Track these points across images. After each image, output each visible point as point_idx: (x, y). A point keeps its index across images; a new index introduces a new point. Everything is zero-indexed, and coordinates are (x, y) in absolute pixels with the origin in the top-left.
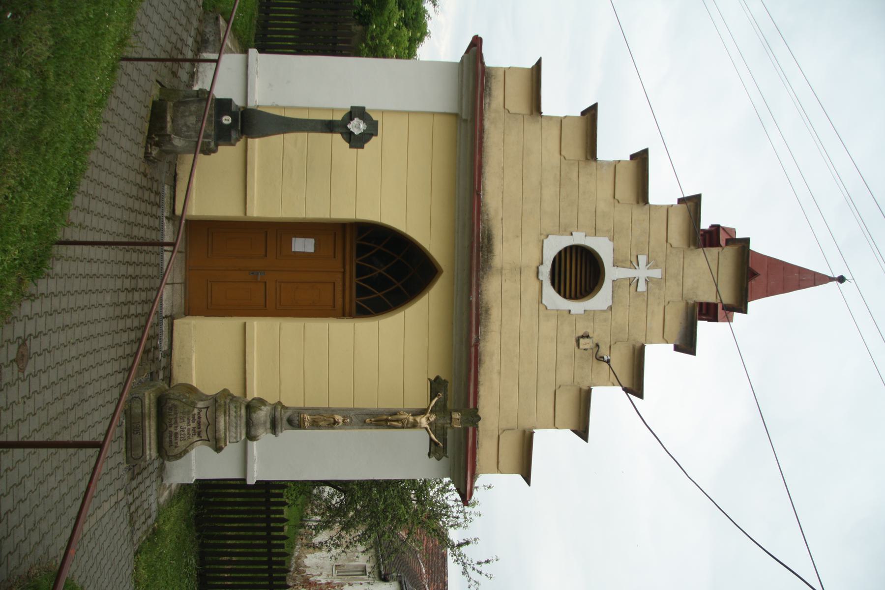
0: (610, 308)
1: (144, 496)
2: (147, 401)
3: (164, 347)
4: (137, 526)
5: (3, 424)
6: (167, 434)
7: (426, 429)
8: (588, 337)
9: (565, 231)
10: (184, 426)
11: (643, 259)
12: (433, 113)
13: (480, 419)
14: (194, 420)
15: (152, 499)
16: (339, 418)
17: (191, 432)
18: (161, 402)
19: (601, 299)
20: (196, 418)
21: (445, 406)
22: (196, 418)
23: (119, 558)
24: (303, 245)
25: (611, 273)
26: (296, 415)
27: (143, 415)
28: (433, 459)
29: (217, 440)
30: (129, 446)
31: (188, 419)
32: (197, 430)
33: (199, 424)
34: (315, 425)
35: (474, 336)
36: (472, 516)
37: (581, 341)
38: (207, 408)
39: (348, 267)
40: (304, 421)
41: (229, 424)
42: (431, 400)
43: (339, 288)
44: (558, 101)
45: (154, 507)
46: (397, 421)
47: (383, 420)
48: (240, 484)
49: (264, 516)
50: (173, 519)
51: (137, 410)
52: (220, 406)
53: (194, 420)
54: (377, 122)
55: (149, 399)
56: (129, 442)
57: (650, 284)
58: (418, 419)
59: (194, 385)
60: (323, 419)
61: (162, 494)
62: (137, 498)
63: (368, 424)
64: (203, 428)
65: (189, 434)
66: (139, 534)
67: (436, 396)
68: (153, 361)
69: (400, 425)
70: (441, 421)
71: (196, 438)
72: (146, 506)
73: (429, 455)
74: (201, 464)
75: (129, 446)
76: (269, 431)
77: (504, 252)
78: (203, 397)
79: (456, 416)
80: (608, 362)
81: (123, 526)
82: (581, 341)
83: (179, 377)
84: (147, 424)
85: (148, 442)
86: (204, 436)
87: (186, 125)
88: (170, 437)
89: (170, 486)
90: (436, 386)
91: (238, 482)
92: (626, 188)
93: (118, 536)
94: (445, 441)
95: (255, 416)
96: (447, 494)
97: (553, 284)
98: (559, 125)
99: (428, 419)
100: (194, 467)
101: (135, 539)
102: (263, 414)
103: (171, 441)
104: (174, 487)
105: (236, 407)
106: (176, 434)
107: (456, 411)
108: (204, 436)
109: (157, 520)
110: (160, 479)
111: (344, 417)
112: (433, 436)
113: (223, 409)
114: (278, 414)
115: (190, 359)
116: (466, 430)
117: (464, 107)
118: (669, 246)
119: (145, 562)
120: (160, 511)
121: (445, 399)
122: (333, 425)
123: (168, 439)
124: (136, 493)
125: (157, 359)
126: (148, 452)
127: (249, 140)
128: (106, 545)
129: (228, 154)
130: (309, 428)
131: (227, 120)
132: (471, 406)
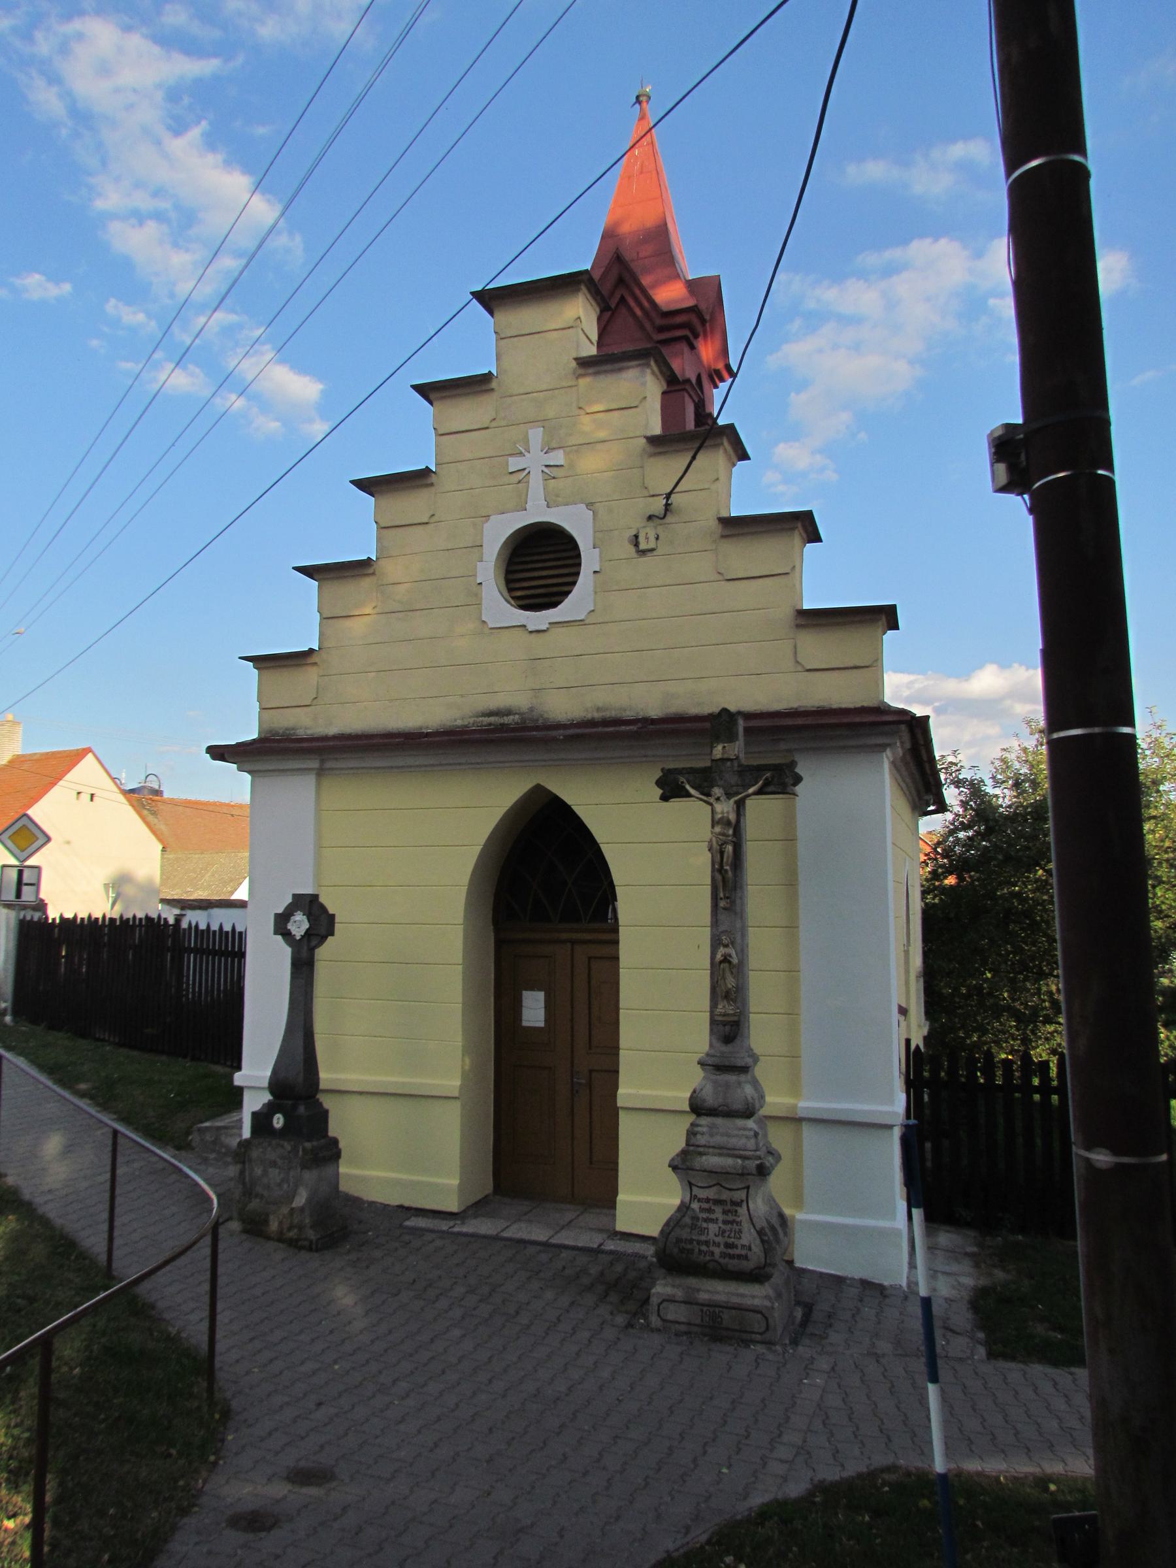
0: (590, 506)
8: (636, 537)
9: (476, 595)
11: (514, 464)
12: (318, 810)
13: (725, 710)
16: (719, 957)
17: (730, 1218)
19: (575, 522)
20: (706, 1206)
22: (706, 1206)
24: (534, 1009)
25: (537, 513)
28: (799, 789)
32: (728, 1207)
33: (718, 1202)
37: (643, 546)
38: (691, 1184)
39: (565, 936)
42: (689, 795)
44: (297, 624)
53: (709, 1211)
54: (294, 896)
57: (554, 445)
63: (733, 903)
64: (726, 1195)
69: (729, 848)
71: (742, 1211)
76: (743, 1078)
77: (509, 691)
80: (668, 496)
82: (643, 546)
86: (742, 1195)
87: (279, 1185)
88: (732, 1257)
92: (411, 505)
94: (761, 769)
97: (554, 605)
98: (330, 621)
99: (718, 799)
103: (739, 1257)
106: (727, 1245)
108: (742, 1195)
117: (389, 764)
118: (494, 424)
122: (739, 970)
126: (757, 1302)
127: (322, 1086)
129: (347, 1122)
131: (278, 1121)
132: (707, 725)
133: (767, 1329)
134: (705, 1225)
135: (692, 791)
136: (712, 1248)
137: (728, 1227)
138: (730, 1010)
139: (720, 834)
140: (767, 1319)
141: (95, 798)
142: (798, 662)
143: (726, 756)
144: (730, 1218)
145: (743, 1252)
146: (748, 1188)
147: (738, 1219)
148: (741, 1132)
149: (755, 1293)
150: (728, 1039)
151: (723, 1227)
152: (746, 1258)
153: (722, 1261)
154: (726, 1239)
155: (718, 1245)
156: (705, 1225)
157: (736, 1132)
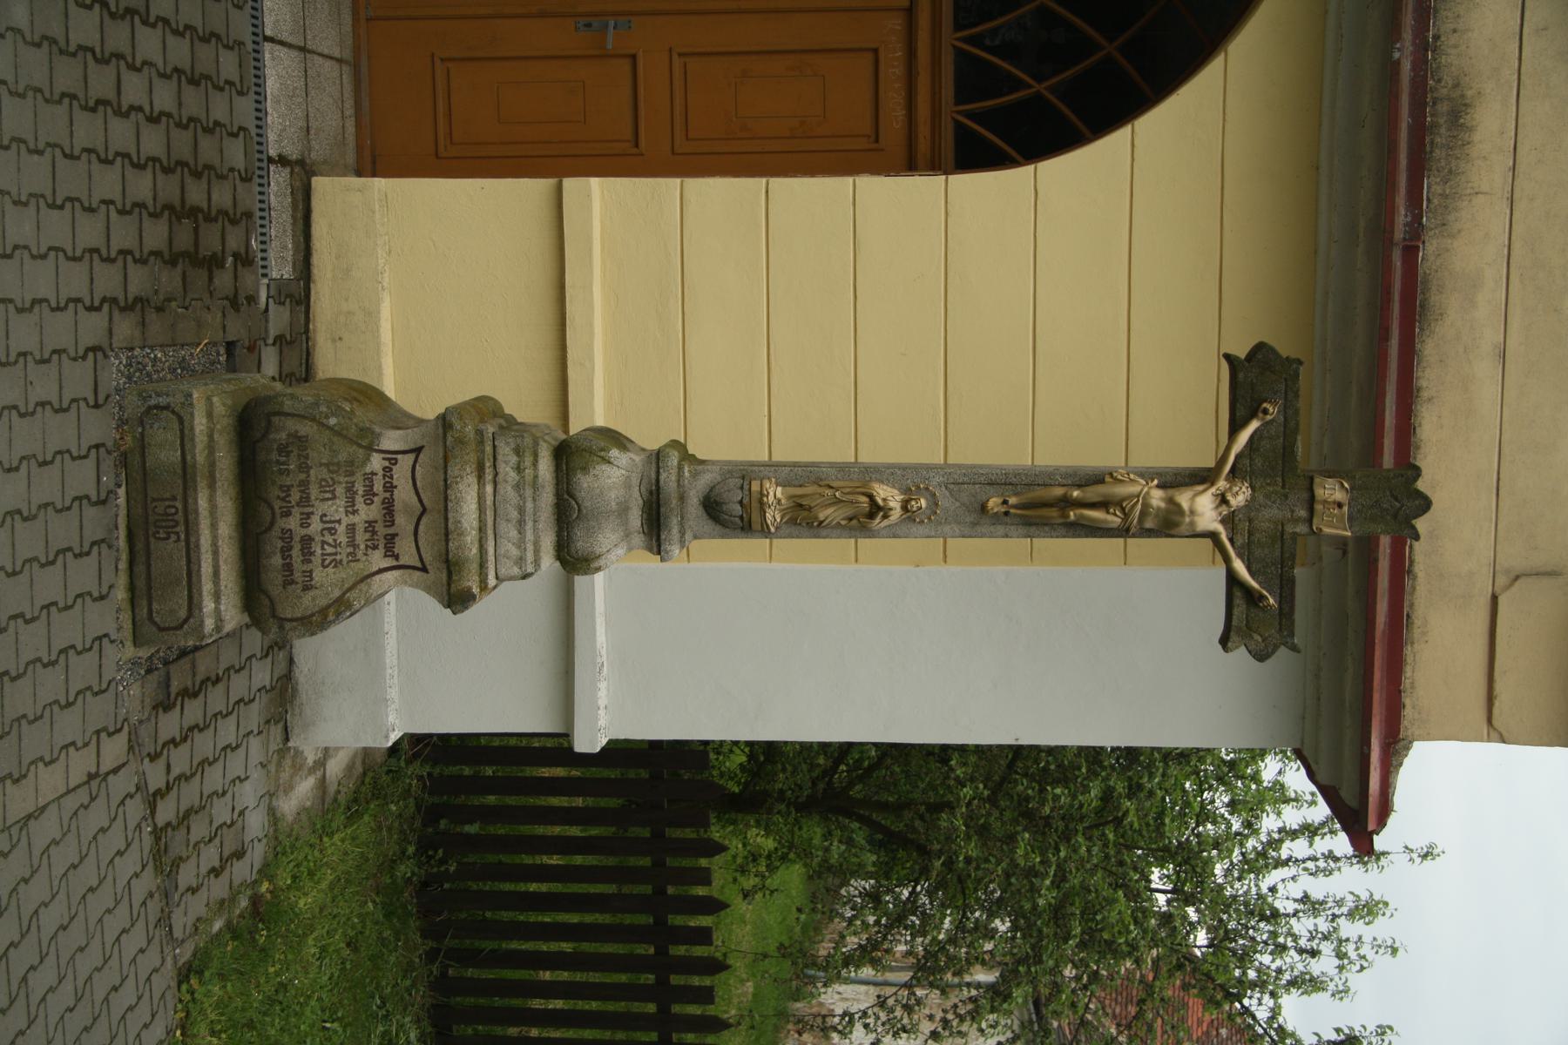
1: (214, 778)
2: (200, 423)
3: (281, 268)
4: (186, 876)
5: (10, 713)
6: (274, 542)
7: (1213, 536)
10: (335, 515)
14: (370, 494)
15: (248, 794)
16: (883, 492)
17: (361, 537)
18: (251, 426)
20: (378, 487)
21: (1288, 452)
22: (378, 487)
23: (111, 976)
26: (734, 482)
27: (186, 471)
28: (1241, 654)
29: (451, 566)
30: (141, 583)
31: (350, 490)
32: (381, 530)
33: (389, 507)
34: (802, 520)
35: (1402, 217)
36: (1366, 950)
40: (762, 506)
41: (495, 511)
42: (1235, 428)
43: (893, 69)
45: (256, 823)
46: (1104, 505)
47: (1051, 507)
48: (556, 748)
49: (647, 889)
50: (330, 876)
51: (165, 454)
52: (461, 441)
53: (370, 494)
55: (208, 411)
56: (140, 568)
58: (1184, 498)
59: (390, 390)
60: (834, 504)
61: (289, 788)
62: (184, 778)
64: (403, 523)
65: (352, 543)
66: (197, 906)
67: (1253, 415)
68: (234, 303)
69: (1114, 520)
70: (1272, 513)
71: (378, 560)
72: (221, 812)
73: (1224, 641)
74: (413, 670)
75: (141, 583)
76: (638, 539)
78: (399, 419)
79: (1331, 491)
81: (129, 864)
83: (331, 362)
84: (203, 503)
85: (206, 568)
86: (408, 556)
88: (286, 551)
89: (321, 764)
90: (1253, 379)
91: (550, 743)
93: (104, 898)
95: (589, 492)
96: (1274, 877)
99: (1223, 500)
100: (393, 693)
101: (181, 922)
102: (612, 480)
103: (288, 567)
104: (335, 767)
105: (518, 451)
106: (307, 541)
107: (1330, 474)
108: (408, 556)
109: (266, 872)
110: (276, 731)
111: (907, 491)
112: (1239, 566)
113: (473, 457)
114: (669, 480)
115: (372, 316)
116: (1366, 547)
119: (220, 1005)
120: (280, 842)
121: (1289, 428)
122: (866, 518)
123: (277, 560)
124: (180, 760)
125: (252, 299)
126: (209, 605)
128: (50, 919)
130: (779, 533)
132: (1388, 461)
133: (161, 629)
134: (340, 490)
135: (1244, 436)
136: (296, 511)
137: (342, 538)
138: (773, 516)
139: (1146, 505)
140: (176, 628)
141: (1428, 863)
142: (1517, 578)
143: (1318, 507)
144: (361, 537)
145: (297, 576)
146: (424, 569)
147: (360, 554)
148: (530, 547)
149: (224, 600)
150: (712, 507)
151: (341, 529)
152: (288, 582)
153: (276, 532)
154: (318, 538)
155: (305, 524)
156: (340, 490)
157: (529, 536)
